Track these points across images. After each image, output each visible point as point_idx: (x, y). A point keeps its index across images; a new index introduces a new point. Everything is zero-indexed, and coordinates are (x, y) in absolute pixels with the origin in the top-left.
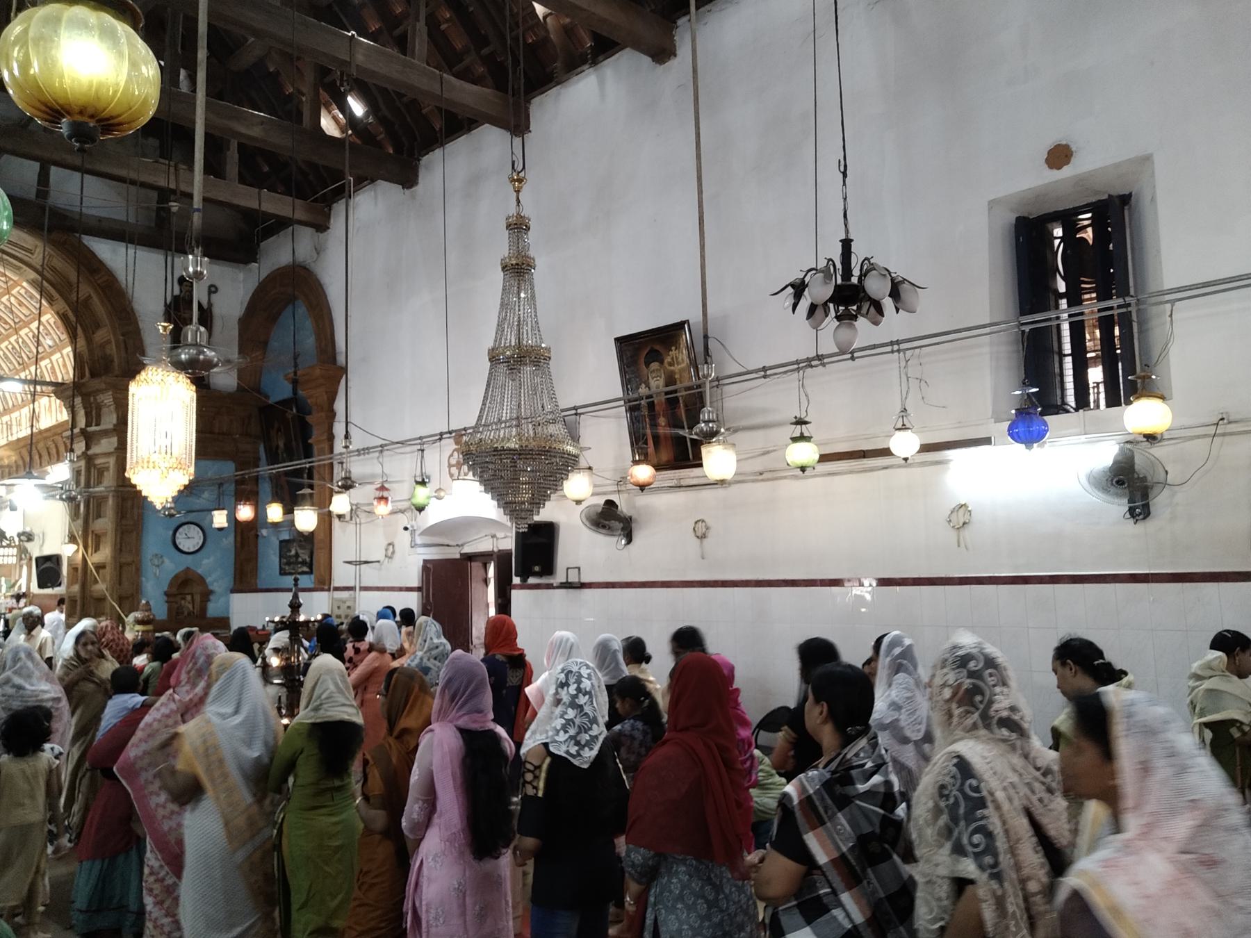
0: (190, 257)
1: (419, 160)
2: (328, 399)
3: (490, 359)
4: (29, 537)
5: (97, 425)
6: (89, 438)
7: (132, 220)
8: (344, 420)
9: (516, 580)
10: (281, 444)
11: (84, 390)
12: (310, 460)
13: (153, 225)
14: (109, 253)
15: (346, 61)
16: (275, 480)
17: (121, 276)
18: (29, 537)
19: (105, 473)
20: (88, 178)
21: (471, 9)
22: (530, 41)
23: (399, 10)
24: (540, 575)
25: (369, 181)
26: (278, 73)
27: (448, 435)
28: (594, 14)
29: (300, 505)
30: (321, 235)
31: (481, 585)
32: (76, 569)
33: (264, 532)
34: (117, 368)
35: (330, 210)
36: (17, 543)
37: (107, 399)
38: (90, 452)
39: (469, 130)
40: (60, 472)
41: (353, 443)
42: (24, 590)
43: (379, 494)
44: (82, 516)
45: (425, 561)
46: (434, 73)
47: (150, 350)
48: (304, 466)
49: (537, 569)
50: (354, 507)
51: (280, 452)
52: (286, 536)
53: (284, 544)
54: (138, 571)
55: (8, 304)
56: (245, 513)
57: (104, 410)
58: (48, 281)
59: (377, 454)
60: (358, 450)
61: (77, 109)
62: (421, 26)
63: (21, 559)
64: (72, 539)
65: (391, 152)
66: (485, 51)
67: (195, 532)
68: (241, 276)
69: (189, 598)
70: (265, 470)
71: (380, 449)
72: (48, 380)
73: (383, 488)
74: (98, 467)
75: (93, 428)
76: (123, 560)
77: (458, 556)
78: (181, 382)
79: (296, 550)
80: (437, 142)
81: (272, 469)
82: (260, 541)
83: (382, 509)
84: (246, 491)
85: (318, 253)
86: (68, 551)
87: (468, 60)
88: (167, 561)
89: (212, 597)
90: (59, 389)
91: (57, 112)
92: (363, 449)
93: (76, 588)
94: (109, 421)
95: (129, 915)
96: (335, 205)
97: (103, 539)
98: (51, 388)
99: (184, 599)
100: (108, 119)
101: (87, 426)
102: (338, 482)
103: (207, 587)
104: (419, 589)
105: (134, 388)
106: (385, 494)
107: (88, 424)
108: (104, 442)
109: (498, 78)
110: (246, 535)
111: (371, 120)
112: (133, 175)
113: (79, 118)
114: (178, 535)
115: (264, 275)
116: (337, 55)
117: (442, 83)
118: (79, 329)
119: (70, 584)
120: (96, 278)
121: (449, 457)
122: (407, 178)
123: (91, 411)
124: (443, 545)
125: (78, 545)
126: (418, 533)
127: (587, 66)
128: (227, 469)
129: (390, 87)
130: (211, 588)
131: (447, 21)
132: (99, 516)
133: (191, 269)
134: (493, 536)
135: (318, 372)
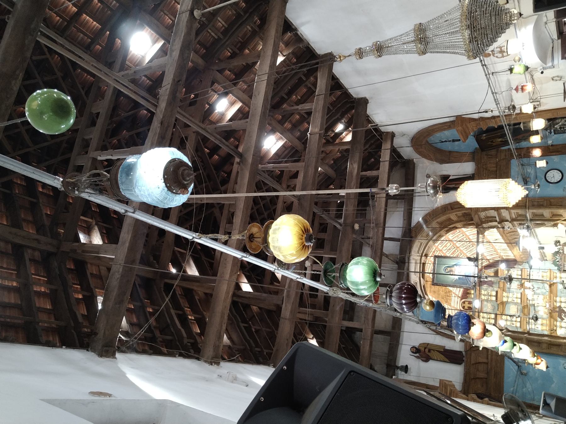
0: (389, 191)
1: (355, 98)
5: (495, 217)
6: (502, 221)
7: (403, 209)
8: (478, 114)
10: (500, 140)
11: (479, 223)
12: (504, 126)
14: (418, 217)
15: (319, 135)
16: (517, 141)
17: (427, 212)
19: (520, 213)
21: (290, 88)
22: (295, 60)
23: (298, 117)
26: (333, 159)
27: (483, 62)
28: (275, 36)
29: (530, 128)
30: (396, 134)
33: (550, 142)
35: (384, 132)
36: (561, 247)
38: (510, 220)
39: (337, 79)
40: (522, 232)
41: (489, 108)
43: (520, 91)
44: (543, 222)
45: (562, 59)
46: (316, 98)
47: (452, 200)
48: (508, 129)
51: (503, 140)
55: (446, 250)
56: (537, 153)
57: (488, 215)
59: (497, 95)
60: (497, 105)
61: (301, 241)
62: (300, 107)
64: (555, 225)
65: (354, 111)
66: (304, 79)
67: (550, 175)
68: (421, 165)
70: (512, 146)
71: (494, 94)
72: (476, 237)
73: (517, 89)
74: (516, 216)
75: (498, 219)
77: (560, 41)
80: (346, 92)
81: (511, 143)
83: (529, 88)
84: (525, 153)
85: (405, 135)
87: (310, 85)
91: (303, 246)
92: (496, 102)
94: (493, 213)
95: (225, 281)
96: (382, 130)
97: (555, 213)
100: (303, 231)
101: (497, 221)
102: (511, 113)
105: (468, 205)
106: (520, 87)
107: (496, 221)
108: (503, 215)
109: (313, 72)
111: (343, 121)
112: (383, 210)
113: (304, 240)
114: (552, 182)
116: (318, 139)
117: (320, 95)
118: (450, 227)
120: (429, 220)
122: (364, 102)
124: (553, 50)
125: (559, 223)
126: (545, 66)
127: (298, 32)
128: (514, 163)
129: (326, 117)
131: (296, 96)
132: (543, 215)
133: (395, 191)
134: (546, 23)
135: (460, 128)
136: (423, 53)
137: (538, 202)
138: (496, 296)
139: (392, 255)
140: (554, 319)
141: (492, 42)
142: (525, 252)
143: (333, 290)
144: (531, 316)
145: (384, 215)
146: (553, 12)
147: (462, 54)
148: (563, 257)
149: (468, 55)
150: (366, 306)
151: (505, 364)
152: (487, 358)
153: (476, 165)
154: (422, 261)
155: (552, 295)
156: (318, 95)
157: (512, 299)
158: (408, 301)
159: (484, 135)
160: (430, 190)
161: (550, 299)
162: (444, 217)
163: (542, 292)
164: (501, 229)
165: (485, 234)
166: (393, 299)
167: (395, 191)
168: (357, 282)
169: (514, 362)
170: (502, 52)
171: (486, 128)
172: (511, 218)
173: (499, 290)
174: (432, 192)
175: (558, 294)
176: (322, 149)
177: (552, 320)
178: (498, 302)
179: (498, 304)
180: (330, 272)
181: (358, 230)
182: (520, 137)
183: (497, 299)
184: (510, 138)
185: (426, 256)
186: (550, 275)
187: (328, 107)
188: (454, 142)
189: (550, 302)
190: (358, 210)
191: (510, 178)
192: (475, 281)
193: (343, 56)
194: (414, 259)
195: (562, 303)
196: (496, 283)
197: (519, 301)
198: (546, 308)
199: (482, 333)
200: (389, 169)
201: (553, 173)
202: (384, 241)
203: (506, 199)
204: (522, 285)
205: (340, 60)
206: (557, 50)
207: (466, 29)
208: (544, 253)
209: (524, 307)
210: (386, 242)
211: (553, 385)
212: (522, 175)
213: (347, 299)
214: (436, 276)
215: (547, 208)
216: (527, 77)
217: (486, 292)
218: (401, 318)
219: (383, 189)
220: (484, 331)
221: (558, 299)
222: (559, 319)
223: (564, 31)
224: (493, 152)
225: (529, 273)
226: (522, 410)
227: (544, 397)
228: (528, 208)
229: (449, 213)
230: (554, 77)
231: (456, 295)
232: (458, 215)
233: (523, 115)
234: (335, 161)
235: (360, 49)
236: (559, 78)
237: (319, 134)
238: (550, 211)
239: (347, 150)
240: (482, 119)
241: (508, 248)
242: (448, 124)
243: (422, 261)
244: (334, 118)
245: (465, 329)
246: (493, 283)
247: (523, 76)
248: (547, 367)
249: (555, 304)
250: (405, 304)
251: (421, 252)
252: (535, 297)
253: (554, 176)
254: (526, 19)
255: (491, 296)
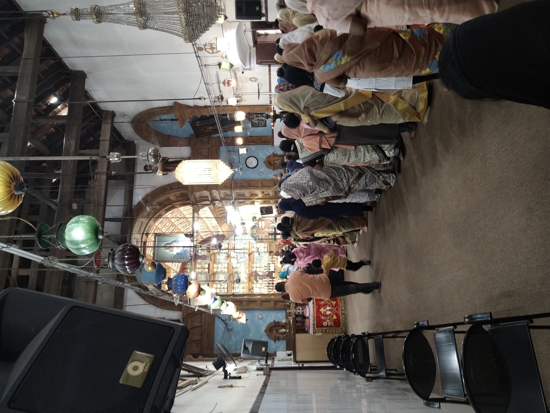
0: (111, 159)
1: (71, 70)
2: (189, 108)
3: (145, 29)
4: (254, 218)
5: (208, 197)
9: (263, 19)
10: (211, 128)
11: (195, 202)
13: (124, 181)
14: (138, 196)
18: (254, 218)
20: (109, 203)
24: (260, 7)
25: (87, 94)
30: (117, 114)
31: (268, 37)
32: (264, 202)
33: (249, 134)
34: (185, 192)
35: (105, 111)
36: (257, 222)
37: (197, 194)
38: (219, 199)
40: (229, 208)
42: (274, 219)
43: (227, 85)
44: (244, 201)
45: (257, 64)
49: (257, 8)
50: (235, 96)
51: (214, 128)
52: (250, 125)
53: (253, 125)
54: (265, 180)
56: (240, 141)
57: (202, 195)
58: (154, 216)
60: (208, 94)
61: (8, 189)
63: (263, 220)
64: (253, 203)
67: (249, 161)
68: (141, 147)
69: (275, 162)
70: (221, 135)
73: (224, 83)
76: (261, 186)
77: (255, 48)
78: (181, 166)
79: (255, 120)
82: (252, 135)
83: (233, 83)
84: (231, 142)
85: (125, 115)
86: (258, 205)
88: (261, 171)
89: (275, 153)
90: (196, 211)
91: (12, 195)
92: (208, 92)
93: (271, 201)
96: (102, 109)
97: (252, 193)
98: (196, 215)
99: (276, 163)
100: (11, 178)
101: (209, 201)
103: (271, 155)
104: (270, 66)
105: (185, 183)
106: (226, 82)
107: (208, 200)
108: (214, 194)
110: (249, 141)
111: (57, 93)
112: (104, 187)
113: (13, 188)
114: (250, 167)
115: (139, 138)
117: (27, 59)
119: (270, 203)
121: (209, 53)
122: (81, 76)
123: (203, 200)
130: (272, 153)
132: (244, 195)
133: (116, 159)
134: (245, 31)
136: (143, 27)
137: (241, 184)
138: (209, 268)
139: (113, 235)
140: (252, 282)
141: (205, 31)
142: (231, 228)
143: (49, 259)
144: (235, 279)
145: (105, 194)
146: (250, 22)
147: (179, 36)
148: (258, 230)
149: (185, 37)
150: (87, 276)
151: (215, 325)
152: (201, 322)
153: (191, 150)
154: (143, 240)
155: (250, 263)
156: (25, 59)
157: (221, 269)
158: (130, 262)
159: (198, 122)
160: (151, 159)
161: (249, 266)
162: (164, 197)
163: (243, 261)
164: (212, 206)
165: (199, 212)
166: (116, 261)
167: (116, 159)
168: (76, 241)
169: (222, 320)
170: (212, 48)
171: (200, 116)
172: (220, 197)
173: (211, 262)
174: (153, 160)
175: (255, 261)
176: (32, 121)
177: (250, 283)
178: (210, 274)
179: (210, 275)
180: (45, 234)
181: (76, 210)
182: (227, 126)
183: (209, 270)
184: (219, 127)
185: (147, 234)
186: (249, 246)
187: (39, 76)
188: (173, 121)
189: (249, 268)
190: (76, 188)
191: (219, 159)
192: (191, 255)
193: (57, 13)
194: (135, 238)
195: (257, 268)
196: (208, 257)
197: (226, 270)
198: (246, 274)
199: (197, 292)
200: (109, 149)
201: (251, 160)
202: (105, 222)
203: (217, 177)
204: (229, 256)
205: (54, 16)
206: (253, 56)
207: (183, 12)
208: (245, 228)
209: (230, 275)
210: (106, 223)
211: (250, 335)
212: (228, 160)
213: (65, 269)
214: (157, 249)
215: (247, 189)
216: (232, 74)
217: (200, 265)
218: (123, 287)
219: (105, 157)
220: (199, 290)
221: (255, 265)
222: (255, 282)
223: (258, 41)
224: (205, 139)
225: (234, 245)
226: (220, 92)
227: (244, 343)
228: (234, 189)
229: (168, 194)
230: (251, 78)
231: (175, 271)
232: (177, 195)
233: (228, 108)
234: (49, 136)
235: (77, 9)
236: (255, 80)
237: (28, 103)
238: (250, 191)
239: (63, 126)
240: (196, 107)
241: (218, 225)
242: (167, 109)
243: (143, 240)
244: (47, 89)
245: (183, 289)
246: (206, 257)
247: (229, 73)
248: (247, 320)
249: (252, 270)
250: (128, 265)
251: (142, 231)
252: (238, 265)
253: (252, 162)
254: (231, 23)
255: (204, 268)
